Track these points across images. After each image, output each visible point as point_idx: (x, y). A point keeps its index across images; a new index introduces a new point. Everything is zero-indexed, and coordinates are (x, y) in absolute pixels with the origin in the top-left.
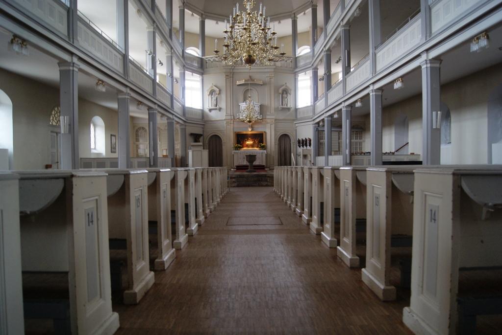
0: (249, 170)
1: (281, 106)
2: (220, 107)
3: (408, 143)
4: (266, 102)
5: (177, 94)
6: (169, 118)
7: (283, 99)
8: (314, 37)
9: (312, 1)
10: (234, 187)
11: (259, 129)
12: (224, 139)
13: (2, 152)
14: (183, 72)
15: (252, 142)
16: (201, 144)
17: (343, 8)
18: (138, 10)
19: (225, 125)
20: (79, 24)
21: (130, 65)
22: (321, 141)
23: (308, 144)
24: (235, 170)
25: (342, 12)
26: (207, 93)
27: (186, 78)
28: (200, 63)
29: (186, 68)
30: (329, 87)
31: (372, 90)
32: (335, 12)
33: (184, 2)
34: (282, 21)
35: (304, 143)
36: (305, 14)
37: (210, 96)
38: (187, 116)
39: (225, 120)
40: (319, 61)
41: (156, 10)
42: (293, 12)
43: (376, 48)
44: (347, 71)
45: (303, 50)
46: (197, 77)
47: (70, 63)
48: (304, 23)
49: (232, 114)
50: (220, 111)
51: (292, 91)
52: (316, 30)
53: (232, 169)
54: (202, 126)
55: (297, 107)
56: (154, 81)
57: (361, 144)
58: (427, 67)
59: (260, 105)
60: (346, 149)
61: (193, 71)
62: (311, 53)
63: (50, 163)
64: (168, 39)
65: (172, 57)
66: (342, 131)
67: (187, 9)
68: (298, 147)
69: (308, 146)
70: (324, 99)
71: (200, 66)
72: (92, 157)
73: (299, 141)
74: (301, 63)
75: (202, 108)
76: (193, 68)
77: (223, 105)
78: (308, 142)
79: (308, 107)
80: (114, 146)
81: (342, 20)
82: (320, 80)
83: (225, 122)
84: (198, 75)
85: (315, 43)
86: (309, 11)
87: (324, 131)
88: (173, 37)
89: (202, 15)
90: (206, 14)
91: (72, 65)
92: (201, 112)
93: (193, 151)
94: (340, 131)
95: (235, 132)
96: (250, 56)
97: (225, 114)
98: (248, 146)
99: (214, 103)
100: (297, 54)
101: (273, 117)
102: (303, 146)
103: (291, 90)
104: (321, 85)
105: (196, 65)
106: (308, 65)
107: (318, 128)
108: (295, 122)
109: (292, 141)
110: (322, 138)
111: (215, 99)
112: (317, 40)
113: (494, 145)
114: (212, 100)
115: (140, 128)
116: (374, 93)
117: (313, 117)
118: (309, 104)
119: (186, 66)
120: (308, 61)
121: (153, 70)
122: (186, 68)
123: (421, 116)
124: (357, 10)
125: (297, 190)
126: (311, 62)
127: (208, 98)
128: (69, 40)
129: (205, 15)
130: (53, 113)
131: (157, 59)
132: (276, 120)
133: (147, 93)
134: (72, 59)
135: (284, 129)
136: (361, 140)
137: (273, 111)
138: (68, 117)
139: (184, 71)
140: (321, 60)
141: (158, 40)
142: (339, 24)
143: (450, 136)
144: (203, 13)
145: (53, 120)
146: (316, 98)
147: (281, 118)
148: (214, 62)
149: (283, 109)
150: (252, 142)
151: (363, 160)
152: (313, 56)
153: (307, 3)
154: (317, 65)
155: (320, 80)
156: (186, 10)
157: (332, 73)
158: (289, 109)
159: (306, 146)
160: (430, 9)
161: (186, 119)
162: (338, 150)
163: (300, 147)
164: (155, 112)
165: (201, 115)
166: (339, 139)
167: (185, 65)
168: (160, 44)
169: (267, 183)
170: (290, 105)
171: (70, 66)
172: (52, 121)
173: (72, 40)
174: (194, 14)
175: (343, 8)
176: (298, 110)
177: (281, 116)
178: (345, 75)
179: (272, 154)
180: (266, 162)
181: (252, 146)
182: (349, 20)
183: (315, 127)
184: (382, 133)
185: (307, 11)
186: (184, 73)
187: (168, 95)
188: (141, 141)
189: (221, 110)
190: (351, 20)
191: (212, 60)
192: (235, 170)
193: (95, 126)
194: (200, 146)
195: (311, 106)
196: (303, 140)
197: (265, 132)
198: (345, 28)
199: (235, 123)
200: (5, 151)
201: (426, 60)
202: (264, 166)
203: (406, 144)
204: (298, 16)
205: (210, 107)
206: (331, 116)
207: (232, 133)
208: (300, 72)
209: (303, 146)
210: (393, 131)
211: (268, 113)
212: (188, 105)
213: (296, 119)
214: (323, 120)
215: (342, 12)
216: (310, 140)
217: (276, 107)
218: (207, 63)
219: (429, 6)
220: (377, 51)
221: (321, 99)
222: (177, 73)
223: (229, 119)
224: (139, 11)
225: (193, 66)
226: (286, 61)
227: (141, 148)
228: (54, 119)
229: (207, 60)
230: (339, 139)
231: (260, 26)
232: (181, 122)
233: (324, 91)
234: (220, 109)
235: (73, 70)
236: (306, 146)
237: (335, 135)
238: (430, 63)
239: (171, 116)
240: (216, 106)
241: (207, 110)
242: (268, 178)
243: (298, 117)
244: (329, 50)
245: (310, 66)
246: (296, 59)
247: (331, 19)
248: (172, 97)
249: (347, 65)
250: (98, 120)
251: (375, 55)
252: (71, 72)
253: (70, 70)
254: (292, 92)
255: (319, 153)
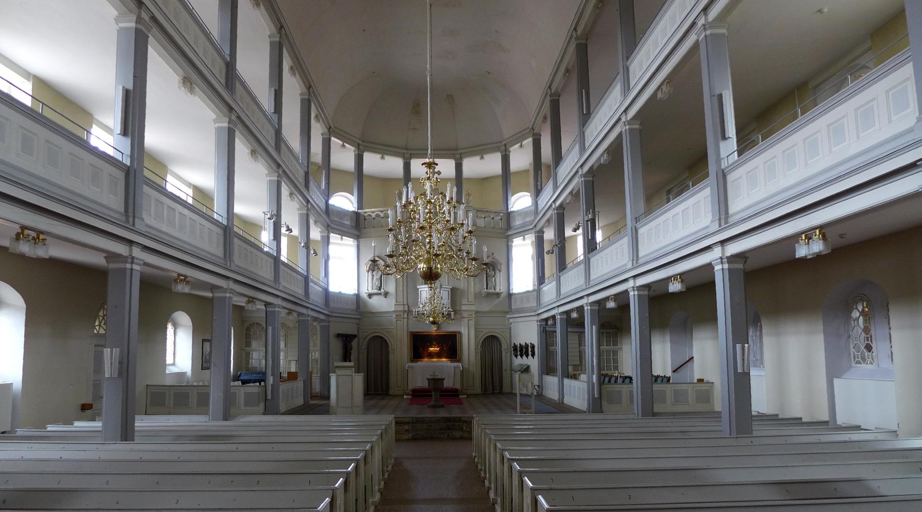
0: (432, 403)
1: (486, 290)
2: (386, 290)
3: (693, 357)
4: (462, 285)
5: (317, 274)
6: (300, 314)
7: (488, 278)
8: (537, 182)
9: (532, 128)
10: (408, 440)
11: (450, 328)
12: (392, 344)
13: (1, 390)
14: (326, 234)
15: (438, 349)
16: (352, 364)
17: (583, 149)
18: (252, 151)
19: (395, 320)
20: (146, 189)
21: (236, 240)
22: (551, 348)
23: (530, 353)
24: (410, 397)
25: (581, 155)
26: (364, 268)
27: (331, 240)
28: (354, 219)
29: (332, 228)
30: (562, 266)
31: (633, 287)
32: (569, 151)
33: (330, 127)
34: (485, 156)
35: (524, 350)
36: (521, 146)
37: (370, 273)
38: (332, 304)
39: (394, 311)
40: (546, 222)
41: (283, 146)
42: (503, 143)
43: (637, 220)
44: (591, 246)
45: (521, 202)
46: (350, 242)
47: (127, 257)
48: (521, 159)
49: (405, 303)
50: (385, 297)
51: (502, 266)
52: (540, 172)
53: (405, 397)
54: (357, 321)
55: (511, 292)
56: (276, 259)
57: (615, 353)
58: (723, 269)
59: (451, 289)
60: (593, 373)
61: (343, 233)
62: (533, 208)
63: (88, 400)
64: (301, 188)
65: (308, 215)
66: (584, 332)
67: (333, 137)
68: (513, 356)
69: (530, 357)
70: (554, 283)
71: (353, 224)
72: (168, 382)
73: (515, 347)
74: (517, 222)
75: (357, 292)
76: (342, 229)
77: (391, 287)
78: (530, 349)
79: (528, 292)
80: (208, 357)
81: (582, 166)
82: (548, 252)
83: (394, 316)
84: (352, 239)
85: (537, 192)
86: (528, 142)
87: (556, 332)
88: (312, 185)
89: (358, 146)
90: (364, 144)
91: (130, 260)
92: (355, 297)
93: (338, 376)
94: (581, 332)
95: (411, 333)
96: (430, 268)
97: (394, 302)
98: (431, 355)
99: (377, 283)
100: (510, 207)
101: (473, 308)
102: (522, 356)
103: (501, 264)
104: (550, 261)
105: (348, 223)
106: (527, 226)
107: (546, 328)
108: (508, 316)
109: (503, 347)
110: (553, 344)
111: (379, 277)
112: (542, 188)
113: (836, 381)
114: (373, 279)
115: (252, 325)
116: (636, 293)
117: (538, 310)
118: (531, 288)
119: (332, 226)
120: (528, 219)
121: (275, 243)
122: (332, 228)
123: (715, 319)
124: (605, 155)
125: (512, 499)
126: (534, 221)
127: (367, 278)
128: (127, 221)
129: (362, 146)
130: (101, 314)
131: (283, 223)
132: (477, 312)
133: (263, 283)
134: (131, 251)
135: (492, 326)
136: (617, 347)
137: (471, 298)
138: (116, 351)
139: (329, 233)
140: (548, 220)
141: (285, 190)
142: (577, 172)
143: (762, 353)
144: (360, 142)
145: (100, 325)
146: (541, 279)
147: (486, 309)
148: (377, 218)
149: (489, 295)
150: (438, 349)
151: (620, 391)
152: (536, 212)
153: (525, 130)
154: (542, 228)
155: (548, 252)
156: (333, 138)
157: (566, 236)
158: (498, 295)
159: (527, 356)
160: (724, 176)
161: (330, 311)
162: (579, 363)
163: (516, 356)
164: (277, 309)
165: (355, 302)
166: (580, 345)
167: (330, 224)
168: (289, 198)
169: (461, 434)
170: (501, 288)
171: (126, 262)
172: (97, 328)
173: (131, 219)
174: (345, 144)
175: (583, 149)
176: (513, 297)
177: (486, 307)
178: (589, 253)
179: (471, 369)
180: (462, 381)
181: (438, 355)
182: (591, 168)
183: (541, 325)
184: (650, 338)
185: (524, 142)
186: (328, 238)
187: (299, 277)
188: (254, 344)
189: (388, 296)
190: (595, 168)
191: (373, 215)
192: (410, 397)
193: (175, 326)
194: (352, 367)
195: (534, 291)
196: (521, 346)
197: (459, 332)
198: (586, 179)
199: (410, 317)
200: (8, 387)
201: (721, 258)
202: (456, 391)
203: (690, 360)
204: (511, 149)
205: (371, 291)
206: (568, 313)
207: (406, 334)
208: (516, 236)
209: (522, 356)
210: (668, 338)
211: (465, 301)
212: (334, 288)
213: (510, 310)
214: (554, 317)
215: (581, 155)
216: (533, 347)
217: (477, 290)
218: (365, 219)
219: (723, 170)
220: (638, 225)
221: (550, 283)
222: (316, 233)
223: (401, 311)
224: (253, 153)
225: (343, 225)
226: (493, 218)
227: (254, 357)
228: (102, 325)
229: (365, 214)
230: (580, 345)
231: (448, 221)
232: (322, 317)
233: (554, 271)
234: (386, 294)
235: (132, 269)
236: (527, 356)
237: (573, 340)
238: (728, 262)
239: (304, 311)
240: (380, 290)
241: (364, 295)
242: (464, 425)
243: (513, 307)
244: (561, 207)
245: (531, 227)
246: (509, 215)
247: (563, 160)
248: (306, 279)
249: (590, 238)
250: (183, 318)
251: (636, 231)
252: (128, 272)
253: (126, 268)
254: (504, 268)
255: (548, 369)
